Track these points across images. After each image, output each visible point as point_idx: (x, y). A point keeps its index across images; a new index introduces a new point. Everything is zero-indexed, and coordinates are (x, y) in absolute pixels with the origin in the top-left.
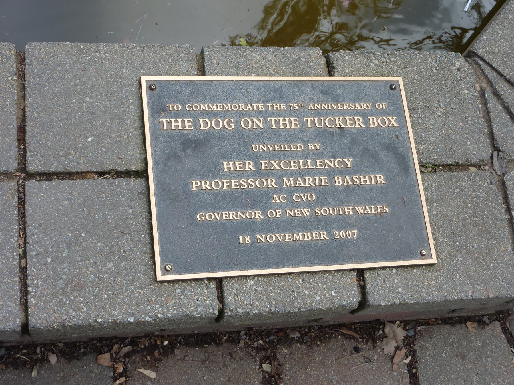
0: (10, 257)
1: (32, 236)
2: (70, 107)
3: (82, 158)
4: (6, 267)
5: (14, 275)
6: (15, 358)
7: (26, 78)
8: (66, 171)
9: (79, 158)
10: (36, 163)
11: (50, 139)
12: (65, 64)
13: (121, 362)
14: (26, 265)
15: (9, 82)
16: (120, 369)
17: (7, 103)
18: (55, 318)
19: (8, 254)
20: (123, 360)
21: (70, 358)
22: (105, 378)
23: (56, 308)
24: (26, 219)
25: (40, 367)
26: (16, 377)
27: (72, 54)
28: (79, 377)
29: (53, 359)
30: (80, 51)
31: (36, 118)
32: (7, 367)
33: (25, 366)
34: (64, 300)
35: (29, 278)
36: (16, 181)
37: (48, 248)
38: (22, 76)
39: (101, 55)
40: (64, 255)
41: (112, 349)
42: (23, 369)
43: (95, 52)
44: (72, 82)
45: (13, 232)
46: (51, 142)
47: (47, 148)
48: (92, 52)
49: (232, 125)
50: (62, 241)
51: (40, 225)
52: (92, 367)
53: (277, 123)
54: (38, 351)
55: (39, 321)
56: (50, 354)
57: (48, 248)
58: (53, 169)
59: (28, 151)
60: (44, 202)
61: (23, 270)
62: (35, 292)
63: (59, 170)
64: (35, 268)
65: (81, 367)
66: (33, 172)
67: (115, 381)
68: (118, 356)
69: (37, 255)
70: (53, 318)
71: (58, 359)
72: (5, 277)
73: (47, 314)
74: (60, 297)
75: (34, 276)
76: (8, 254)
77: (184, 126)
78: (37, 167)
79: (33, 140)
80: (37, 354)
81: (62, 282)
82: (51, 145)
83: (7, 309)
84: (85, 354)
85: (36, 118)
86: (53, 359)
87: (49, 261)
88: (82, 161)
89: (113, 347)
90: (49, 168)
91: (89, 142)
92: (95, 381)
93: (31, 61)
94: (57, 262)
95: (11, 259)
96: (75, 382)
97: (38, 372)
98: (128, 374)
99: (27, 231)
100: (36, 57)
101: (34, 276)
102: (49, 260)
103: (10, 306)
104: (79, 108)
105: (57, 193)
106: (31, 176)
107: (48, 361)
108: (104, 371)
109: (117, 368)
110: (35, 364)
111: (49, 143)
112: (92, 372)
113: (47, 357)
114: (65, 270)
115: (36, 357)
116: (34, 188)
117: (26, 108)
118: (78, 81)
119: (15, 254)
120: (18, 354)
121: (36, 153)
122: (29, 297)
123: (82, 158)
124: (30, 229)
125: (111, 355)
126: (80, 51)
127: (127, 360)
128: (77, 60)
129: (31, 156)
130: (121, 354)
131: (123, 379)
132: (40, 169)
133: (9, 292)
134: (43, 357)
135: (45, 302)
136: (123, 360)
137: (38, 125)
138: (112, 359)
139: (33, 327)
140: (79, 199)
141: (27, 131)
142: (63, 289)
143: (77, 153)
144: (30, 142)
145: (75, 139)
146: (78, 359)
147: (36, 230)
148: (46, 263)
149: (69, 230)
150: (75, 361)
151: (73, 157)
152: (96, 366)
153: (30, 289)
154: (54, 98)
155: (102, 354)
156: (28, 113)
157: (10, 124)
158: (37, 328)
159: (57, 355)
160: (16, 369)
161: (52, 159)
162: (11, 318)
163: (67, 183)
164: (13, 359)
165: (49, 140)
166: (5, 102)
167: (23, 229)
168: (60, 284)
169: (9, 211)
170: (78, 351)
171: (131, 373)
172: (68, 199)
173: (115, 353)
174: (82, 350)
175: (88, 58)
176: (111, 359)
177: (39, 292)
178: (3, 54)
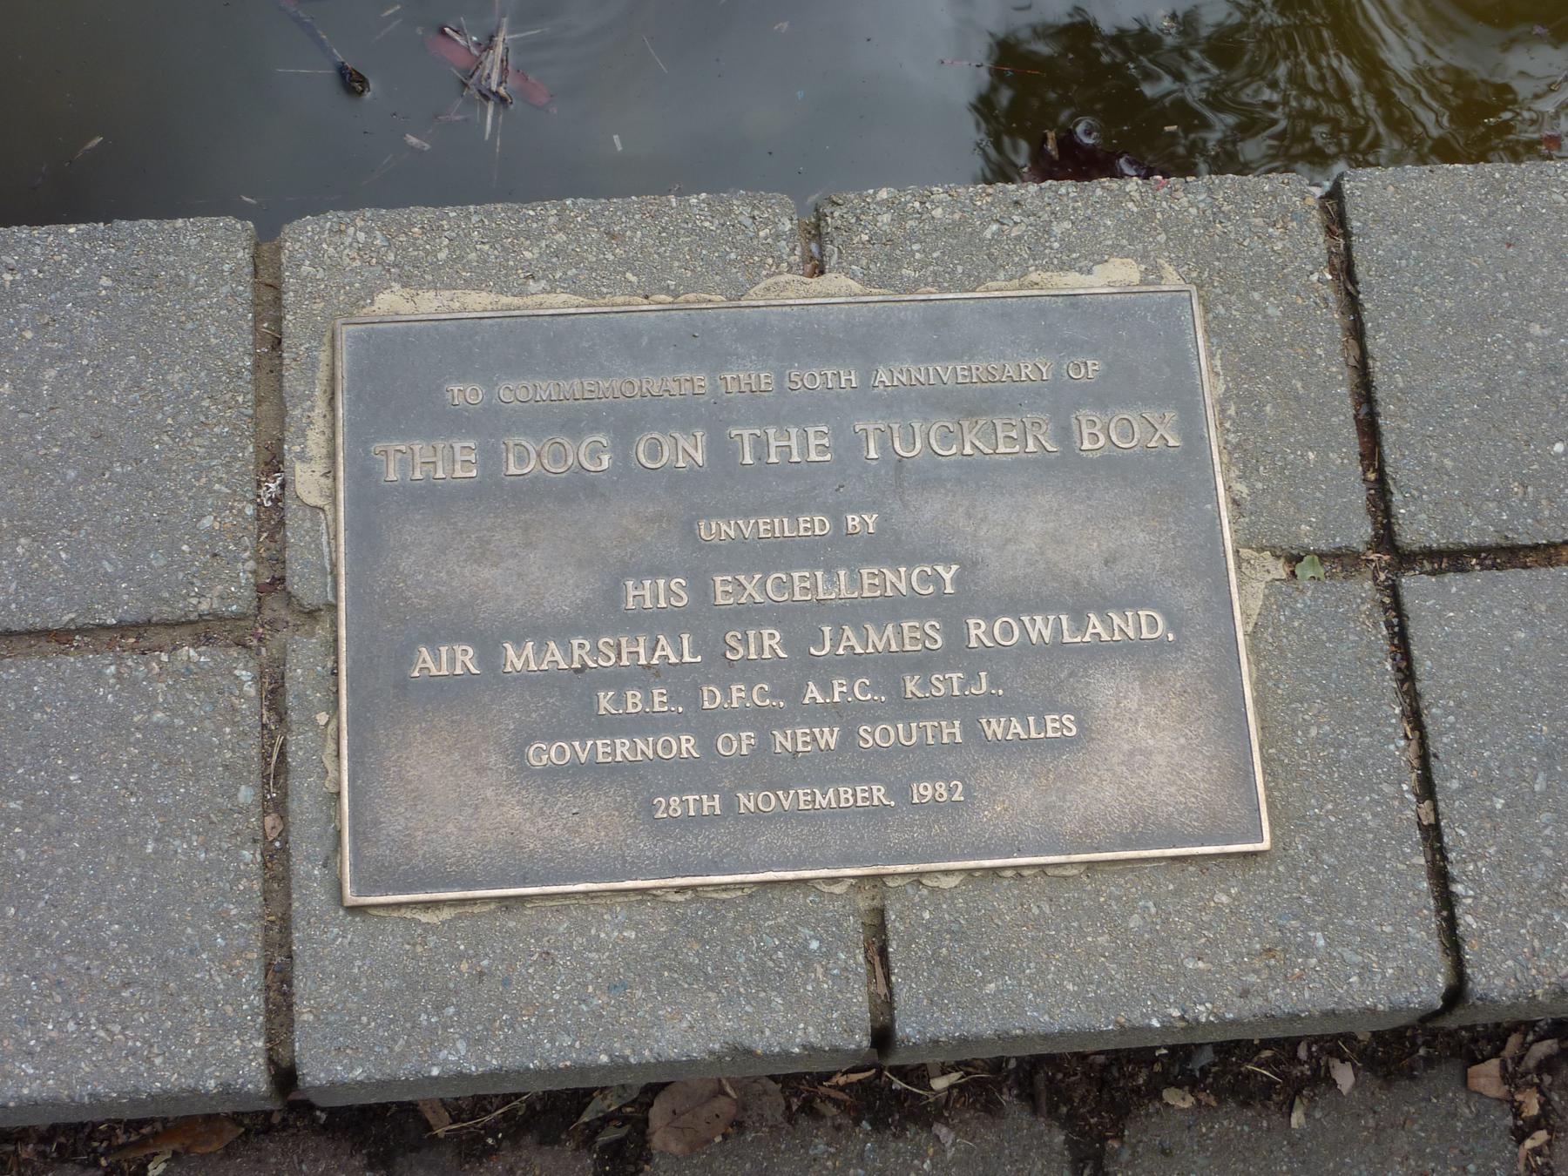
0: (1394, 798)
1: (1441, 734)
2: (1490, 354)
3: (1544, 502)
4: (1388, 826)
5: (1411, 847)
6: (1240, 1073)
7: (1359, 277)
8: (1504, 543)
9: (1537, 502)
10: (1421, 523)
11: (1448, 450)
12: (1461, 229)
13: (1531, 1085)
14: (1438, 821)
15: (1309, 288)
16: (1532, 1108)
17: (1319, 351)
18: (1540, 972)
19: (1386, 788)
20: (1536, 1080)
21: (1390, 1073)
22: (1492, 1132)
23: (1536, 943)
24: (1418, 686)
25: (1311, 1100)
26: (1246, 1128)
27: (1472, 198)
28: (1421, 1130)
29: (1344, 1076)
30: (1495, 188)
31: (1401, 391)
32: (1220, 1101)
33: (1269, 1098)
34: (1557, 919)
35: (1452, 856)
36: (1370, 575)
37: (1491, 770)
38: (1345, 270)
39: (1555, 197)
40: (1537, 788)
41: (1503, 1048)
42: (1264, 1106)
43: (1537, 189)
44: (1486, 279)
45: (1391, 725)
46: (1454, 459)
47: (1446, 478)
48: (1529, 189)
49: (605, 458)
50: (1525, 748)
51: (1460, 704)
52: (1452, 1100)
53: (761, 445)
54: (1302, 1053)
55: (1498, 982)
56: (1336, 1062)
57: (1491, 770)
58: (1471, 539)
59: (1393, 489)
60: (1459, 636)
61: (1432, 834)
62: (1475, 898)
63: (1489, 540)
64: (1464, 829)
65: (1423, 1099)
66: (1415, 548)
67: (1520, 1142)
68: (1521, 1069)
69: (1466, 788)
70: (1534, 972)
71: (1356, 1076)
72: (1388, 855)
73: (1516, 960)
74: (1544, 911)
75: (1464, 852)
76: (1386, 788)
77: (804, 450)
78: (1427, 534)
79: (1404, 456)
80: (1301, 1063)
81: (1542, 866)
82: (1456, 468)
83: (1407, 946)
84: (1429, 1062)
85: (1401, 391)
86: (1344, 1076)
87: (1499, 806)
88: (1547, 513)
89: (1505, 1042)
90: (1460, 537)
91: (1557, 456)
92: (1466, 1142)
93: (1365, 223)
94: (1522, 809)
95: (1396, 803)
96: (1410, 1144)
97: (1307, 1115)
98: (1554, 1120)
99: (1427, 720)
100: (1376, 211)
101: (1464, 852)
102: (1499, 804)
103: (1414, 939)
104: (1517, 357)
105: (1491, 608)
106: (1405, 559)
107: (1333, 1084)
108: (1487, 1112)
109: (1521, 1103)
110: (1298, 1092)
111: (1448, 462)
112: (1455, 1115)
113: (1328, 1070)
114: (1547, 832)
115: (1296, 1072)
116: (1426, 597)
117: (1370, 362)
118: (1501, 276)
119: (1405, 787)
120: (1249, 1061)
121: (1416, 493)
122: (1459, 911)
123: (1544, 502)
124: (1433, 714)
125: (1504, 1067)
126: (1495, 188)
127: (1547, 1079)
128: (1491, 214)
129: (1406, 505)
130: (1530, 1062)
131: (1541, 1136)
132: (1435, 539)
133: (1404, 898)
134: (1316, 1070)
135: (1506, 923)
136: (1536, 1080)
137: (1410, 410)
138: (1507, 1077)
139: (1480, 999)
140: (1553, 624)
141: (1383, 429)
142: (1547, 886)
143: (1530, 489)
144: (1396, 460)
145: (1518, 450)
146: (1412, 1078)
147: (1451, 719)
148: (1491, 814)
149: (1539, 715)
150: (1404, 1083)
151: (1521, 501)
152: (1463, 1096)
153: (1458, 888)
154: (1443, 330)
155: (1477, 1062)
156: (1379, 378)
157: (1335, 413)
158: (1493, 1001)
159: (1354, 1066)
160: (1245, 1104)
161: (1462, 509)
162: (1420, 972)
163: (1514, 580)
164: (1236, 1076)
165: (1447, 455)
166: (1312, 347)
167: (1415, 717)
168: (1538, 873)
169: (1371, 665)
170: (1410, 1055)
171: (1562, 1118)
172: (1525, 624)
173: (1513, 1058)
174: (1422, 1052)
175: (1519, 209)
176: (1503, 1077)
177: (1486, 898)
178: (1285, 207)
